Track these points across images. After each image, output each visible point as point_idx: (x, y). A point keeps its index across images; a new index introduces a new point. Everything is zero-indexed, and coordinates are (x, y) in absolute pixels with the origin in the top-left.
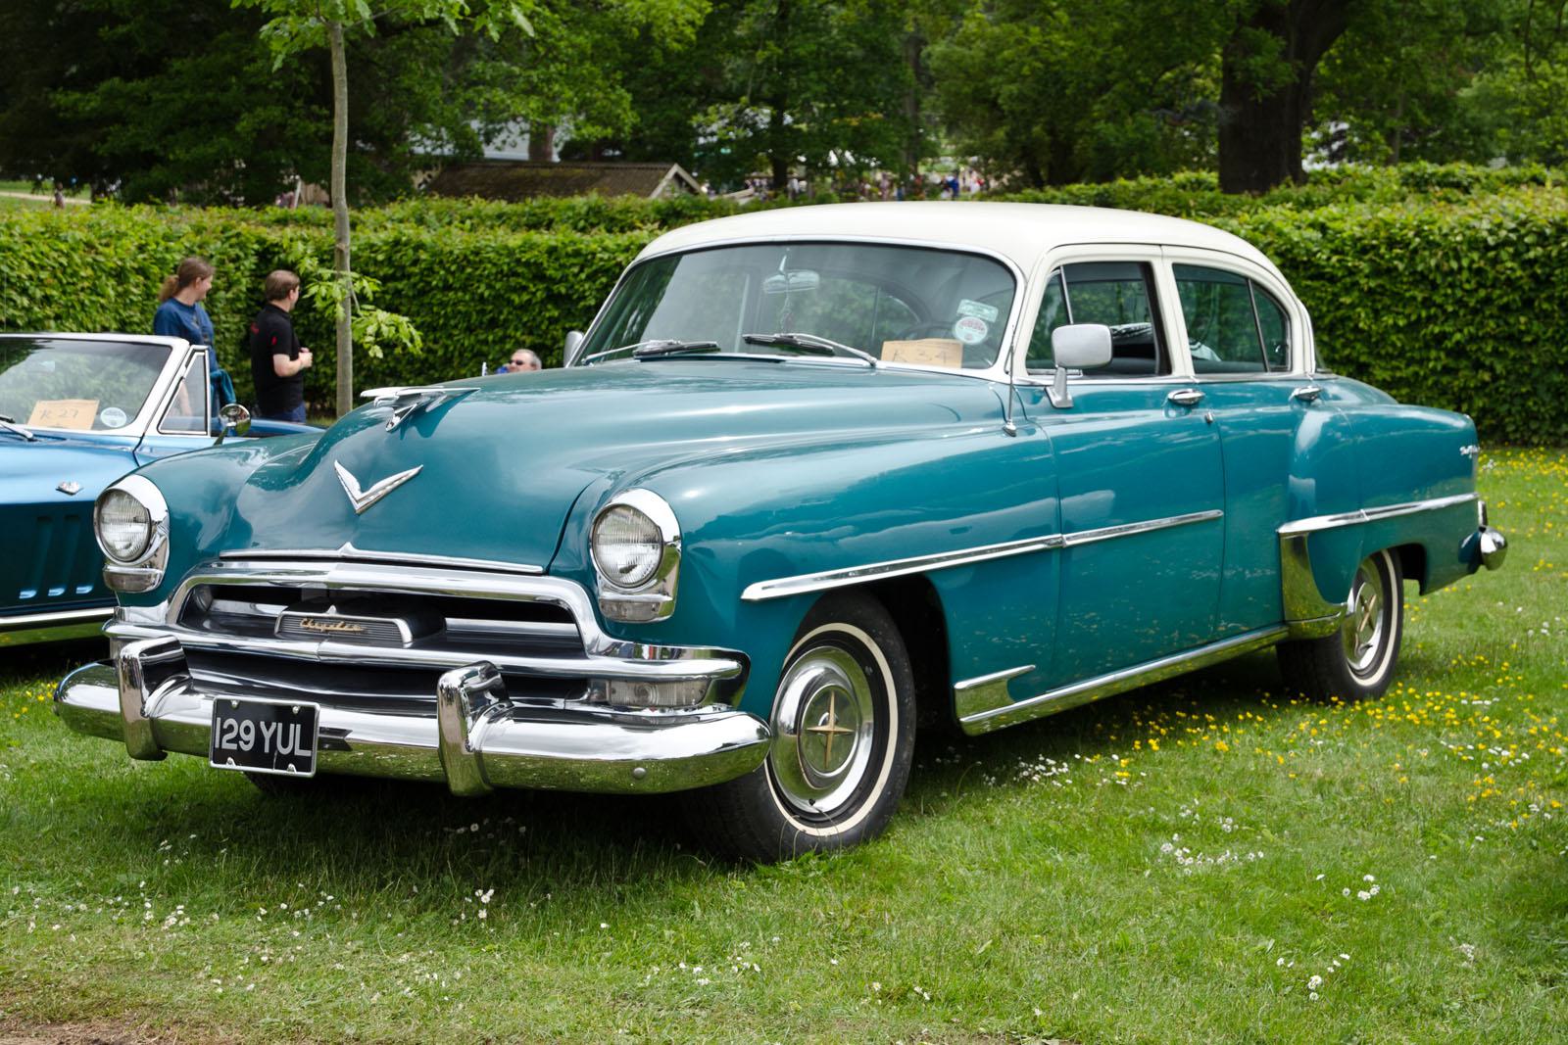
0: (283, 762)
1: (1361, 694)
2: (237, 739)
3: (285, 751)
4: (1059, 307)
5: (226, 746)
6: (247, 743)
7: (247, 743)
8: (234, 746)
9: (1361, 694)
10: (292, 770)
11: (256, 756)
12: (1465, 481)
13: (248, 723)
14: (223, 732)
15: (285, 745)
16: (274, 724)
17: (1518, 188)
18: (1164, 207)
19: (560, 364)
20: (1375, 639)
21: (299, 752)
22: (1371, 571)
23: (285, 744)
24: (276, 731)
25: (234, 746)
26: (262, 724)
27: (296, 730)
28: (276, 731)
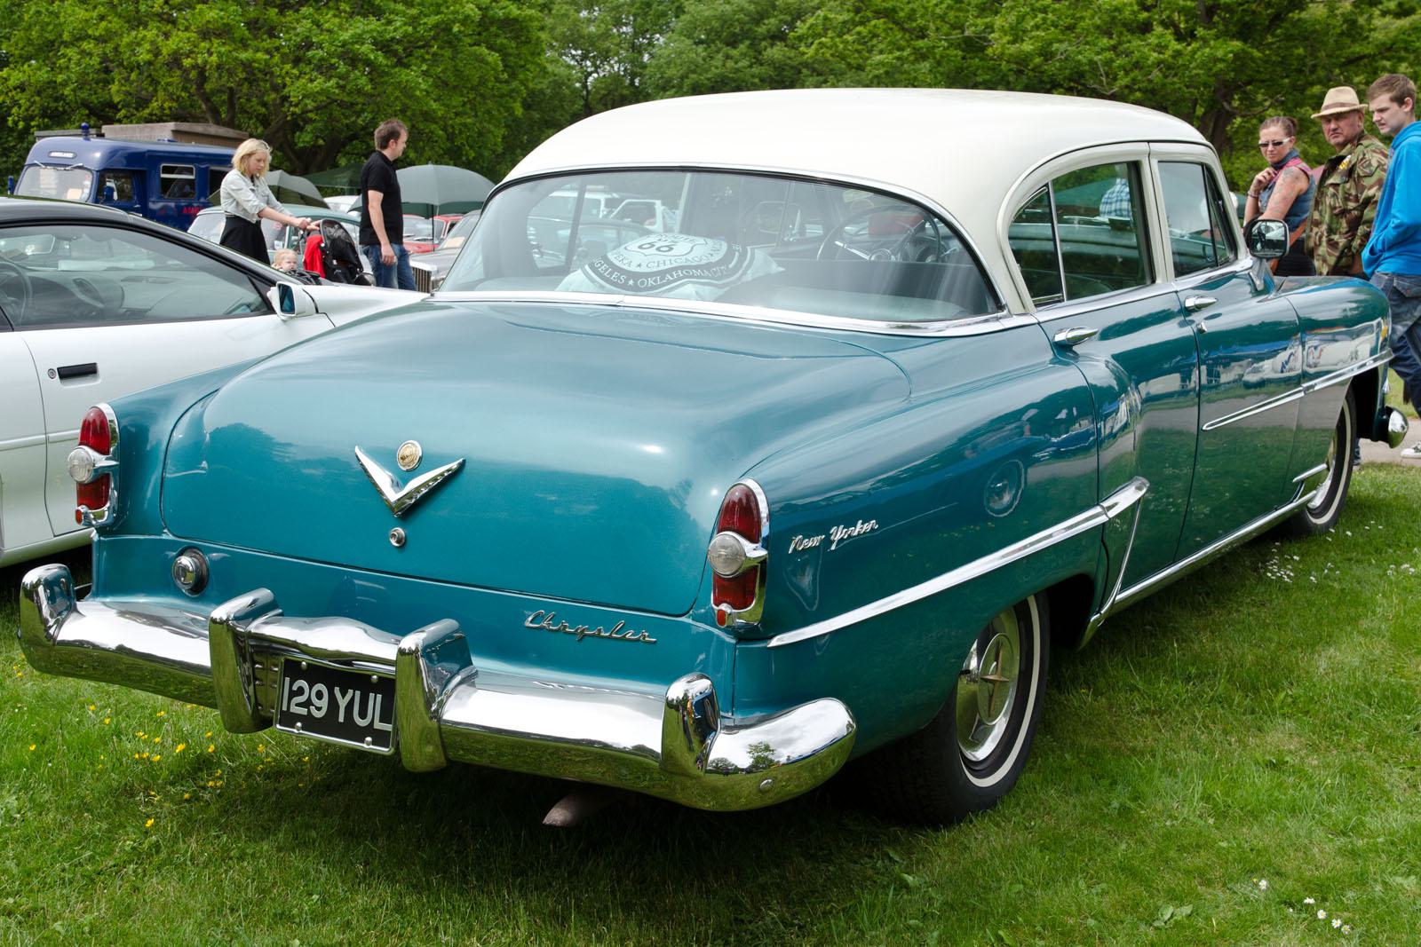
0: (359, 734)
1: (989, 801)
2: (308, 704)
3: (362, 723)
4: (1189, 264)
5: (295, 709)
6: (319, 709)
7: (319, 709)
8: (304, 711)
9: (989, 801)
10: (367, 745)
11: (327, 724)
12: (652, 220)
13: (320, 687)
14: (292, 694)
15: (363, 715)
16: (351, 691)
17: (322, 89)
18: (514, 126)
19: (219, 203)
20: (1000, 725)
21: (378, 725)
22: (1009, 628)
23: (363, 715)
24: (352, 700)
25: (304, 711)
26: (337, 690)
27: (375, 701)
28: (352, 700)
